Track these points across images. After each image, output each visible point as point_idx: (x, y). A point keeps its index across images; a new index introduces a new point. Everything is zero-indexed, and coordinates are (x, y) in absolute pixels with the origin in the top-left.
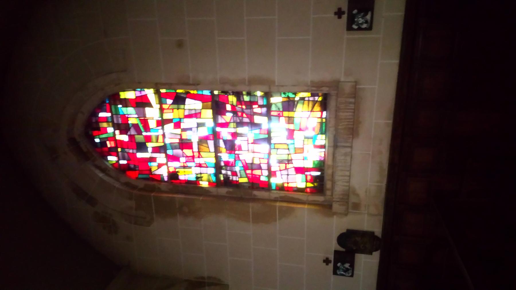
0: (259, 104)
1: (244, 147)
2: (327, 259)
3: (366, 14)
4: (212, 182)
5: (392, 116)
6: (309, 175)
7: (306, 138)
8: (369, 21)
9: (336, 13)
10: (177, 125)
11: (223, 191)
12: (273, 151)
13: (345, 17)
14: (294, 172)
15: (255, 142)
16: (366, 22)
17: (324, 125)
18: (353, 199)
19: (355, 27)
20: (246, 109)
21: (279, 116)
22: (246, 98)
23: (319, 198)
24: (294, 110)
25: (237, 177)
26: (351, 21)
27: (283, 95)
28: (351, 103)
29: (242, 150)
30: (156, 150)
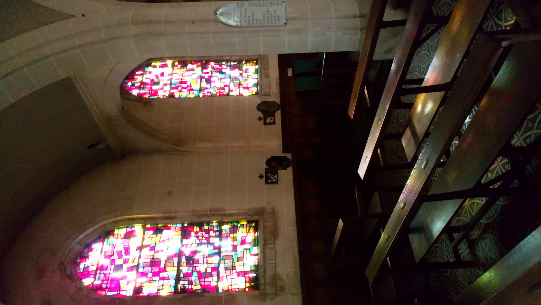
0: (214, 230)
1: (201, 261)
2: (261, 175)
3: (275, 175)
4: (181, 232)
5: (295, 225)
6: (248, 277)
7: (245, 249)
8: (276, 178)
9: (259, 177)
10: (153, 248)
11: (180, 296)
12: (222, 262)
13: (264, 179)
14: (237, 276)
15: (209, 256)
16: (275, 179)
17: (256, 241)
18: (280, 283)
19: (269, 181)
20: (205, 234)
21: (227, 237)
22: (206, 227)
23: (257, 292)
24: (237, 232)
25: (192, 285)
26: (267, 178)
27: (230, 224)
28: (271, 217)
29: (199, 263)
30: (130, 269)
